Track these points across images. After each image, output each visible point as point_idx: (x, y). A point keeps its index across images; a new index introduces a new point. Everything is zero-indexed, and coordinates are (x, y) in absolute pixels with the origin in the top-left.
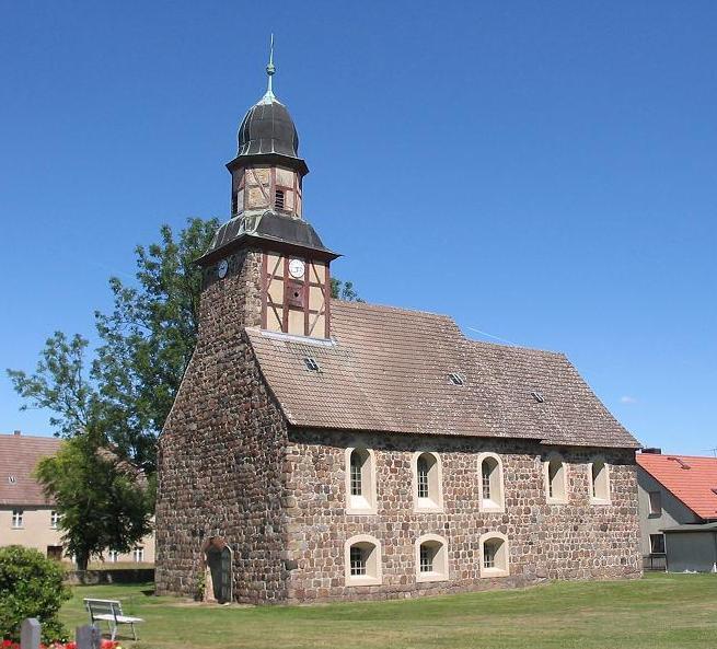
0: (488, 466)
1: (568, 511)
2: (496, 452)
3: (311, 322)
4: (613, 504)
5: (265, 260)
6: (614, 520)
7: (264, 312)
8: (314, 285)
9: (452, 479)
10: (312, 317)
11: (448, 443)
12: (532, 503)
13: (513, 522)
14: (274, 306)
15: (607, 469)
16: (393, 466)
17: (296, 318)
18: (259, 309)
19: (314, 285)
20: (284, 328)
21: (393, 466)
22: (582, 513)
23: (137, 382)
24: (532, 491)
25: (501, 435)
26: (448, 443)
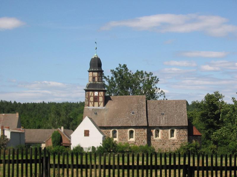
0: (131, 132)
1: (161, 141)
2: (134, 129)
3: (100, 104)
4: (178, 139)
5: (89, 93)
6: (177, 143)
7: (89, 104)
8: (92, 102)
9: (121, 134)
10: (100, 103)
11: (161, 128)
12: (144, 139)
13: (137, 143)
14: (91, 102)
15: (160, 131)
16: (106, 133)
17: (96, 104)
18: (88, 103)
19: (100, 96)
20: (94, 106)
21: (106, 133)
22: (166, 141)
23: (39, 83)
24: (143, 137)
25: (133, 125)
26: (161, 128)
